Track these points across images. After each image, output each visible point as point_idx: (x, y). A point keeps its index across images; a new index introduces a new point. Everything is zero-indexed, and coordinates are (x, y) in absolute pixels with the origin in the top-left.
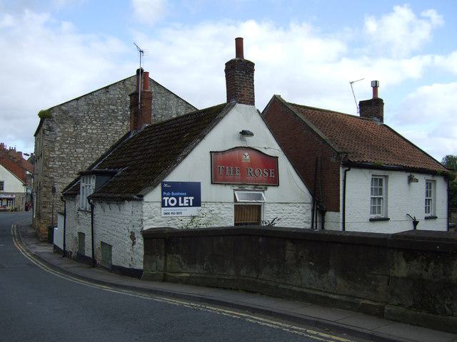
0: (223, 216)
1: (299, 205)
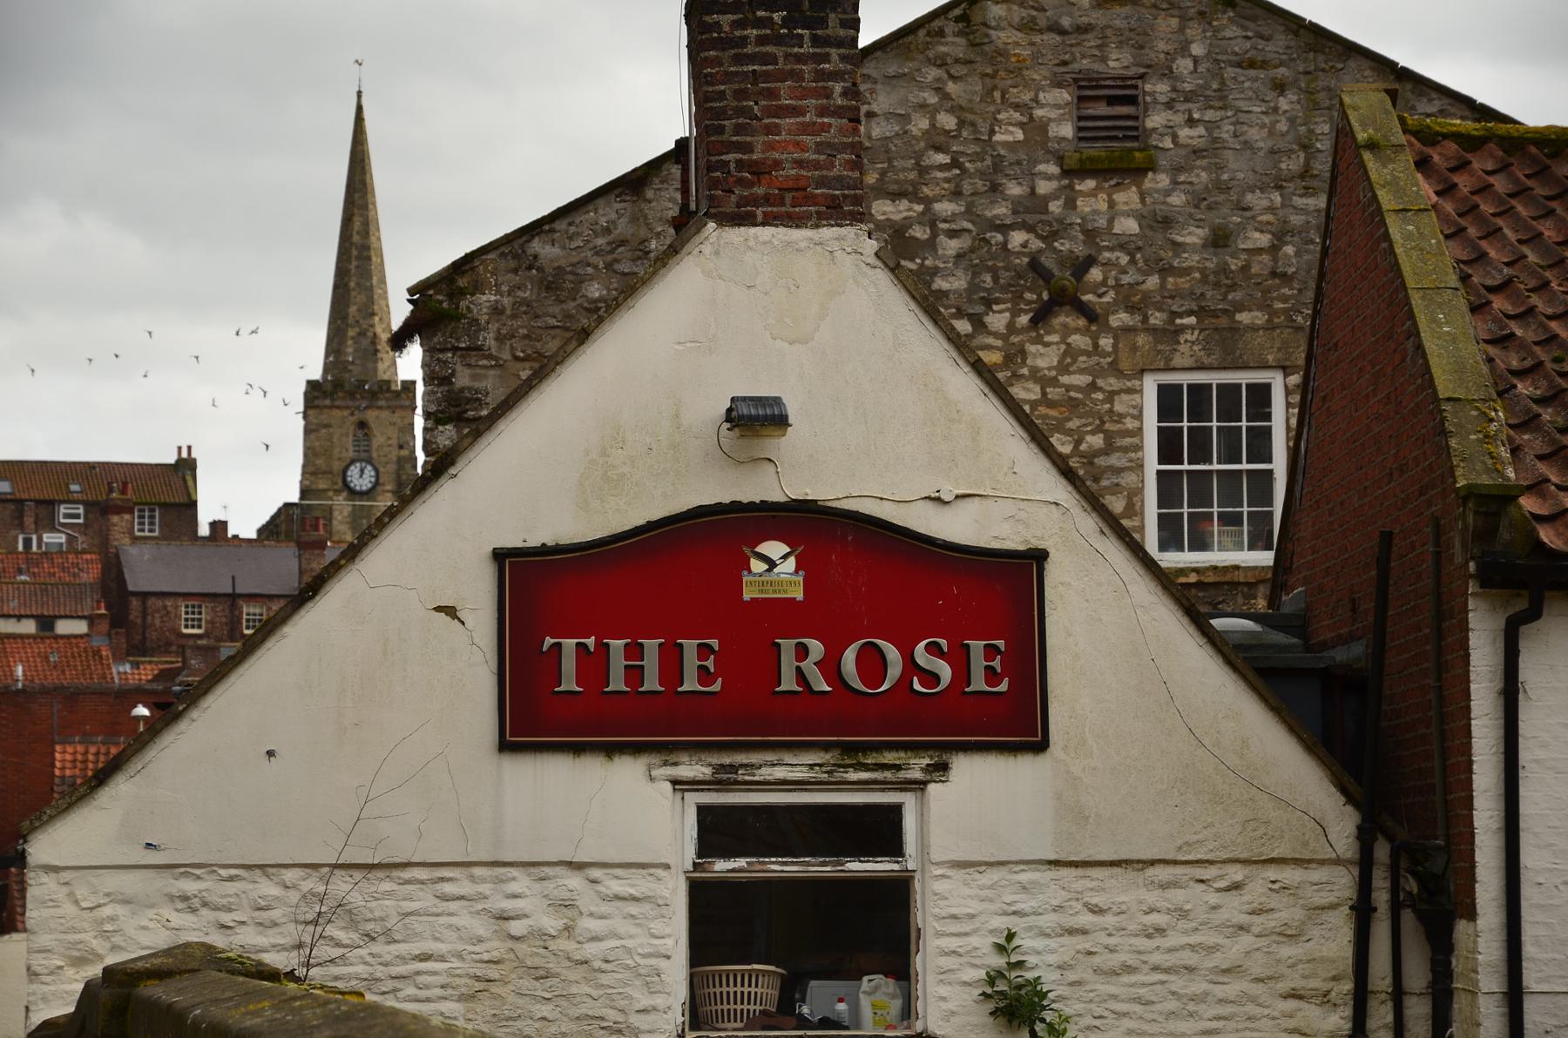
0: (591, 950)
1: (1237, 873)
